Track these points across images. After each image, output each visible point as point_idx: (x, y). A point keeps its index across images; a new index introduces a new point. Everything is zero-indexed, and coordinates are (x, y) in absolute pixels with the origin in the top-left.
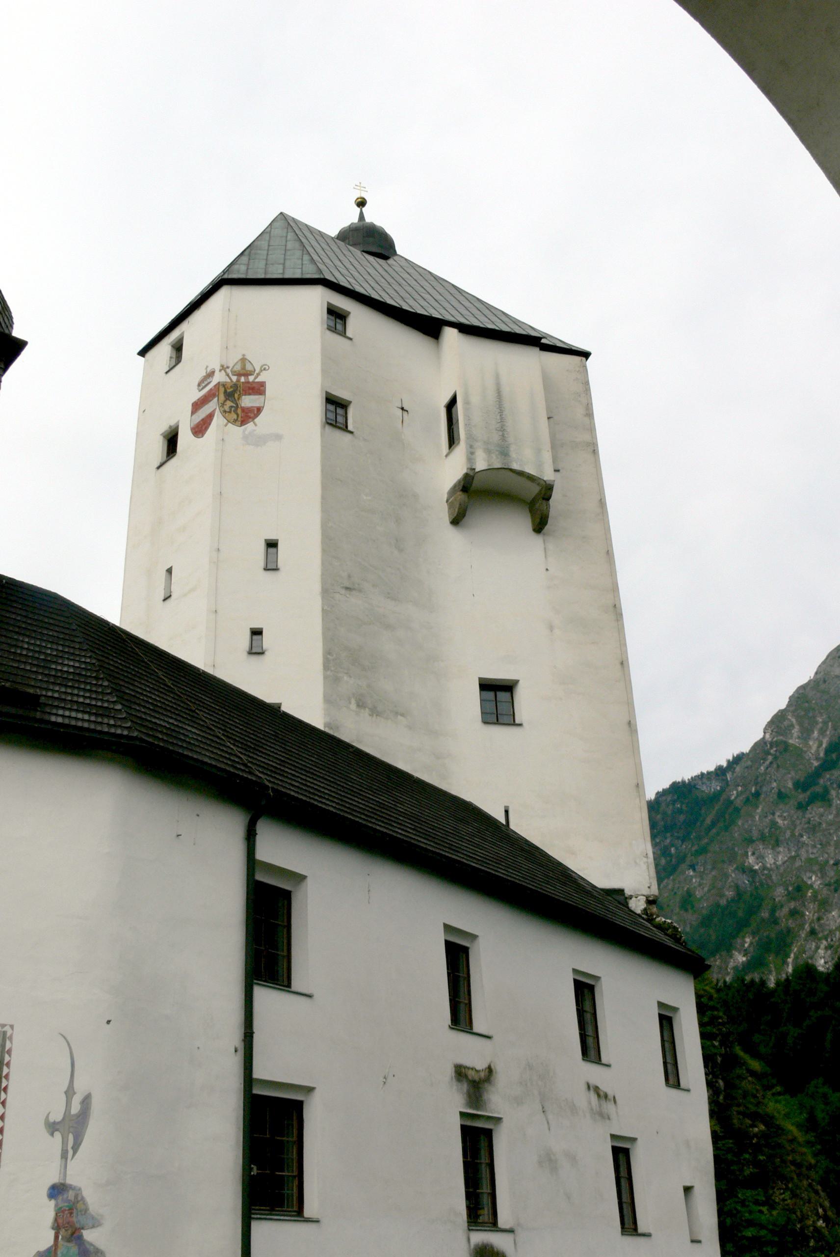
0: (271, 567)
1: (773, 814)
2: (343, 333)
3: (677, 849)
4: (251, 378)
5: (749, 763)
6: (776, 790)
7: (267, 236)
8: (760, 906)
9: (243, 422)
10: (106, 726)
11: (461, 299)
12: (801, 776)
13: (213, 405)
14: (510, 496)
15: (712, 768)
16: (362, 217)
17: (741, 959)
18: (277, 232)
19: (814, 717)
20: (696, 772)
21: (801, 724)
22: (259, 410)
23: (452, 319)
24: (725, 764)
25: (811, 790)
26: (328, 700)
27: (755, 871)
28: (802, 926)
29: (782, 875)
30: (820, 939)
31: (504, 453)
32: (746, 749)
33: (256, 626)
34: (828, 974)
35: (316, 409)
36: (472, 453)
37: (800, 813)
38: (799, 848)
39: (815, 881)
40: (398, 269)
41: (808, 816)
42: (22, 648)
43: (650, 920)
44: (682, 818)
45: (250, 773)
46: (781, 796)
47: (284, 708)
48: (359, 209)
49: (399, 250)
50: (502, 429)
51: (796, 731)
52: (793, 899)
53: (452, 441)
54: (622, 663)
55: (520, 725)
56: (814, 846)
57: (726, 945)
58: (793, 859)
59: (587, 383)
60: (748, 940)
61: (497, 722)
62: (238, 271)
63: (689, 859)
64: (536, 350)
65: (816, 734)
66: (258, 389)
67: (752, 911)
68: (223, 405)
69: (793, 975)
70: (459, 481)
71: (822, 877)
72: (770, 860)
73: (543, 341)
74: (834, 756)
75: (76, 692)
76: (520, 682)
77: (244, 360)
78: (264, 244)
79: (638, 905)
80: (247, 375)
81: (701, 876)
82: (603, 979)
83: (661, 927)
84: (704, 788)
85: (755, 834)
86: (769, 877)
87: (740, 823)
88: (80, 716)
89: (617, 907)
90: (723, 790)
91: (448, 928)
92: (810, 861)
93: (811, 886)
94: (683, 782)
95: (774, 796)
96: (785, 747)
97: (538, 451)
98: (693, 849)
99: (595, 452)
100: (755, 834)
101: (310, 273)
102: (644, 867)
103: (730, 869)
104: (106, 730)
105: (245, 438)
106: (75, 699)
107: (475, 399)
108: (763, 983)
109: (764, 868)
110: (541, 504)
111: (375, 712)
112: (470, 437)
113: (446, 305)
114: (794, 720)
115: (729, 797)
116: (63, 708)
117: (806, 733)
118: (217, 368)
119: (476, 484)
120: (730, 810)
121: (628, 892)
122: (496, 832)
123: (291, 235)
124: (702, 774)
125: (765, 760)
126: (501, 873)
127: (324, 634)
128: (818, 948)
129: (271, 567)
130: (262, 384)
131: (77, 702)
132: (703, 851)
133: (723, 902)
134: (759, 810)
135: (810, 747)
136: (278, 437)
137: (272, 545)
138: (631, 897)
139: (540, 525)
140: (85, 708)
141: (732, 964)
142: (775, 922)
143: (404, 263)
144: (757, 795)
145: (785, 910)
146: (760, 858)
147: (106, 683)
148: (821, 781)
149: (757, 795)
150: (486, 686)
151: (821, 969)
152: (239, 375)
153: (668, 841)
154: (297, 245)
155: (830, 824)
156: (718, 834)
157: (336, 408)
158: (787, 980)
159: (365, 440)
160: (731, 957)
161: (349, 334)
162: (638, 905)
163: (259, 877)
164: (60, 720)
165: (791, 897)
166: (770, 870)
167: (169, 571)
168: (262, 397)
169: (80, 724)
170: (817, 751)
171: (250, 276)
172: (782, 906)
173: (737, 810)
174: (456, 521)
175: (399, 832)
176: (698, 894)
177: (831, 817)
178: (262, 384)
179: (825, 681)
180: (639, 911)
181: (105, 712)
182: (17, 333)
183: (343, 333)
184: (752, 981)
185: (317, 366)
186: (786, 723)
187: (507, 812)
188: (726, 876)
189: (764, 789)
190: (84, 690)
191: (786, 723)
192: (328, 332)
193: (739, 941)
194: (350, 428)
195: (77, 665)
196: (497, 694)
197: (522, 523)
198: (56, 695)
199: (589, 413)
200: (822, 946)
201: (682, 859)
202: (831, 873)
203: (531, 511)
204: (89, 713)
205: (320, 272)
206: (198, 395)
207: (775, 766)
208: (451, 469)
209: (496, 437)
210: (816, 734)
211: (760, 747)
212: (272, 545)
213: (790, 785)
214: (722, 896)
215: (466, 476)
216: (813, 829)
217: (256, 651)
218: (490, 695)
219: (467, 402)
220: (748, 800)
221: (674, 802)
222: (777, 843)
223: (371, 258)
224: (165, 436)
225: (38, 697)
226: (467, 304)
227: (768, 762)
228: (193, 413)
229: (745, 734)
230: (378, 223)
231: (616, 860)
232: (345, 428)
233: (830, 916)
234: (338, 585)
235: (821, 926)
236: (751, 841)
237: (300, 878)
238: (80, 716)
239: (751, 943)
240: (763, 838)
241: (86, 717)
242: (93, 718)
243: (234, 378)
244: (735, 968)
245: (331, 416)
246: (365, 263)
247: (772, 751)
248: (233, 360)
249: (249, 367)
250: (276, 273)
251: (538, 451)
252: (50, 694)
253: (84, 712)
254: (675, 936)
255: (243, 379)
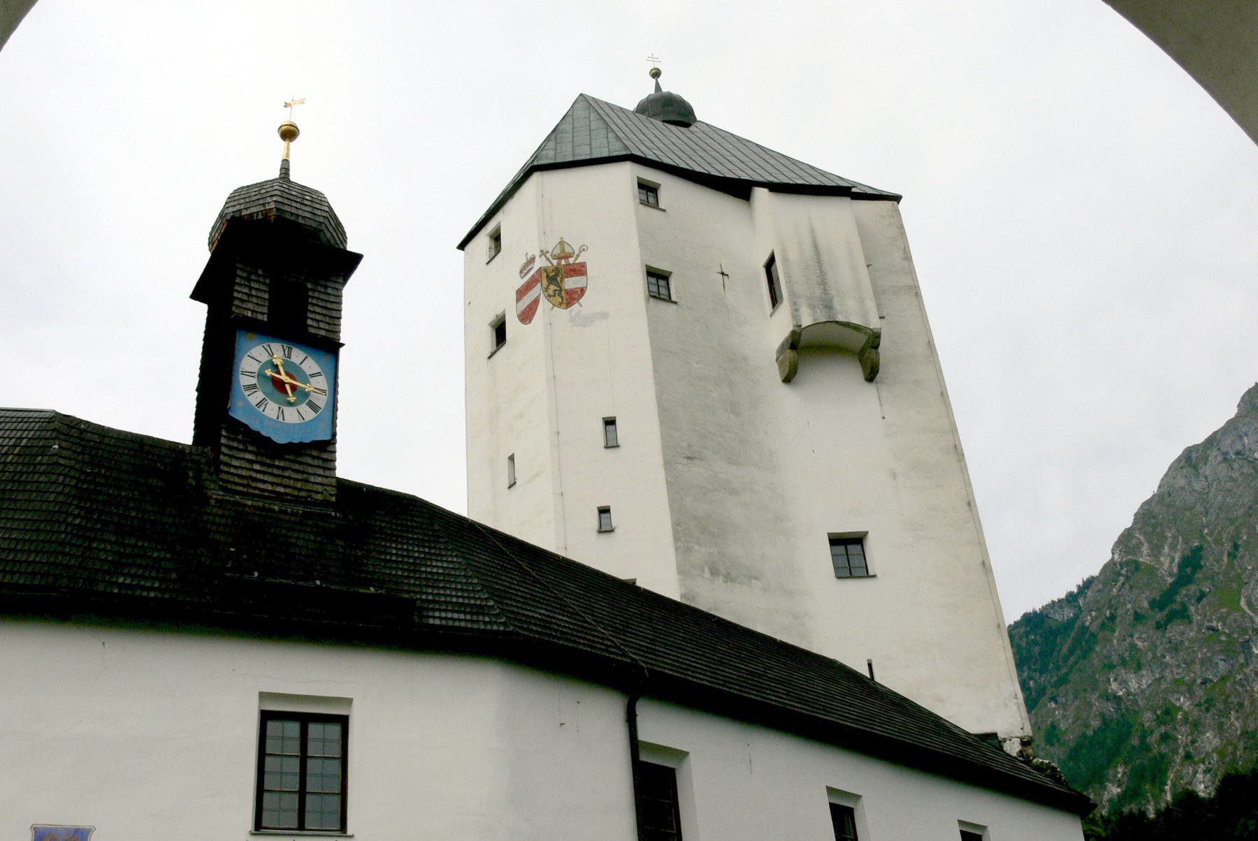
0: (611, 444)
1: (1132, 636)
2: (656, 206)
3: (1035, 682)
4: (571, 260)
5: (1101, 586)
6: (1131, 612)
7: (569, 119)
8: (1128, 733)
9: (569, 305)
10: (482, 623)
11: (767, 157)
12: (1156, 595)
13: (537, 291)
14: (837, 348)
15: (1063, 596)
16: (658, 87)
17: (1116, 790)
18: (581, 113)
19: (1163, 532)
20: (1047, 601)
21: (1149, 542)
22: (583, 291)
23: (761, 179)
24: (1075, 590)
25: (1169, 608)
26: (682, 571)
27: (1120, 698)
28: (1175, 751)
29: (1148, 699)
30: (1196, 763)
31: (829, 307)
32: (1096, 572)
33: (603, 504)
34: (1211, 801)
35: (638, 283)
36: (797, 310)
37: (1159, 634)
38: (1163, 670)
39: (1184, 702)
40: (701, 135)
41: (1168, 635)
42: (392, 554)
43: (1028, 761)
44: (1037, 649)
45: (624, 655)
46: (1138, 617)
47: (638, 584)
48: (654, 81)
49: (699, 116)
50: (823, 282)
51: (1145, 549)
52: (1165, 723)
53: (775, 300)
54: (969, 504)
55: (874, 576)
56: (1179, 666)
57: (1099, 777)
58: (1158, 681)
59: (902, 227)
60: (1120, 770)
61: (851, 576)
62: (547, 157)
63: (1048, 692)
64: (848, 199)
65: (1166, 549)
66: (580, 270)
67: (1122, 738)
68: (547, 289)
69: (1174, 804)
70: (787, 340)
71: (1191, 698)
72: (1133, 685)
73: (854, 190)
74: (1188, 570)
75: (448, 592)
76: (870, 536)
77: (562, 243)
78: (568, 126)
79: (1013, 748)
80: (567, 257)
81: (1065, 707)
82: (989, 829)
83: (1040, 768)
84: (1057, 617)
85: (1115, 659)
86: (1135, 702)
87: (1098, 649)
88: (456, 616)
89: (994, 753)
90: (1076, 617)
91: (831, 791)
92: (1176, 682)
93: (1180, 708)
94: (1035, 612)
95: (1130, 617)
96: (1137, 566)
97: (862, 301)
98: (1053, 680)
99: (918, 295)
100: (1115, 659)
101: (617, 151)
102: (1015, 708)
103: (1093, 698)
104: (482, 627)
105: (572, 319)
106: (449, 599)
107: (793, 256)
108: (1143, 814)
109: (1129, 693)
110: (870, 353)
111: (729, 578)
112: (793, 294)
113: (752, 165)
114: (1142, 538)
115: (1084, 623)
116: (440, 610)
117: (1156, 550)
118: (537, 254)
119: (804, 339)
120: (1087, 636)
121: (1001, 736)
122: (863, 687)
123: (593, 115)
124: (1053, 602)
125: (1116, 581)
126: (878, 730)
127: (671, 506)
128: (1196, 772)
129: (611, 444)
130: (583, 265)
131: (469, 604)
132: (1062, 681)
133: (1090, 733)
134: (1116, 634)
135: (1162, 564)
136: (605, 315)
137: (610, 422)
138: (1005, 740)
139: (871, 374)
140: (461, 608)
141: (1106, 797)
142: (1145, 747)
143: (706, 129)
144: (1112, 618)
145: (1156, 735)
146: (1124, 683)
147: (475, 581)
148: (1178, 598)
149: (1112, 618)
150: (837, 541)
151: (1202, 794)
152: (559, 258)
153: (1026, 674)
154: (601, 124)
155: (1192, 641)
156: (1076, 663)
157: (657, 277)
158: (1167, 809)
159: (690, 309)
160: (1105, 788)
161: (662, 206)
162: (1013, 748)
163: (644, 757)
164: (437, 622)
165: (1160, 721)
166: (1134, 695)
167: (512, 458)
168: (584, 278)
169: (457, 624)
170: (1170, 566)
171: (559, 160)
172: (1152, 732)
173: (1094, 636)
174: (787, 380)
175: (773, 699)
176: (1063, 726)
177: (1192, 634)
178: (583, 265)
179: (1170, 495)
180: (1014, 755)
181: (480, 610)
182: (350, 247)
183: (656, 206)
184: (1131, 813)
185: (635, 241)
186: (1134, 541)
187: (870, 665)
188: (1091, 705)
189: (1120, 612)
190: (456, 589)
191: (1134, 541)
192: (641, 206)
193: (1111, 772)
194: (673, 298)
195: (445, 565)
196: (848, 549)
197: (852, 373)
198: (430, 597)
199: (907, 257)
200: (1200, 770)
201: (1042, 692)
202: (1200, 693)
203: (861, 361)
204: (465, 613)
205: (626, 147)
206: (520, 282)
207: (1127, 586)
208: (778, 328)
209: (818, 291)
210: (1166, 549)
211: (1110, 570)
212: (610, 422)
213: (1146, 605)
214: (1087, 727)
215: (793, 333)
216: (1175, 648)
217: (605, 530)
218: (841, 549)
219: (785, 260)
220: (1103, 624)
221: (1027, 633)
222: (1139, 667)
223: (672, 127)
224: (492, 325)
225: (413, 601)
226: (773, 162)
227: (1119, 584)
228: (518, 301)
229: (1094, 558)
230: (675, 92)
231: (985, 702)
232: (669, 299)
233: (1205, 737)
234: (680, 454)
235: (1195, 749)
236: (1111, 667)
237: (683, 755)
238: (456, 616)
239: (1124, 773)
240: (1124, 663)
241: (462, 616)
242: (468, 617)
243: (555, 262)
244: (1111, 801)
245: (654, 288)
246: (667, 132)
247: (1123, 572)
248: (551, 245)
249: (568, 250)
250: (584, 154)
251: (862, 301)
252: (424, 597)
253: (459, 612)
254: (1053, 774)
255: (563, 262)
